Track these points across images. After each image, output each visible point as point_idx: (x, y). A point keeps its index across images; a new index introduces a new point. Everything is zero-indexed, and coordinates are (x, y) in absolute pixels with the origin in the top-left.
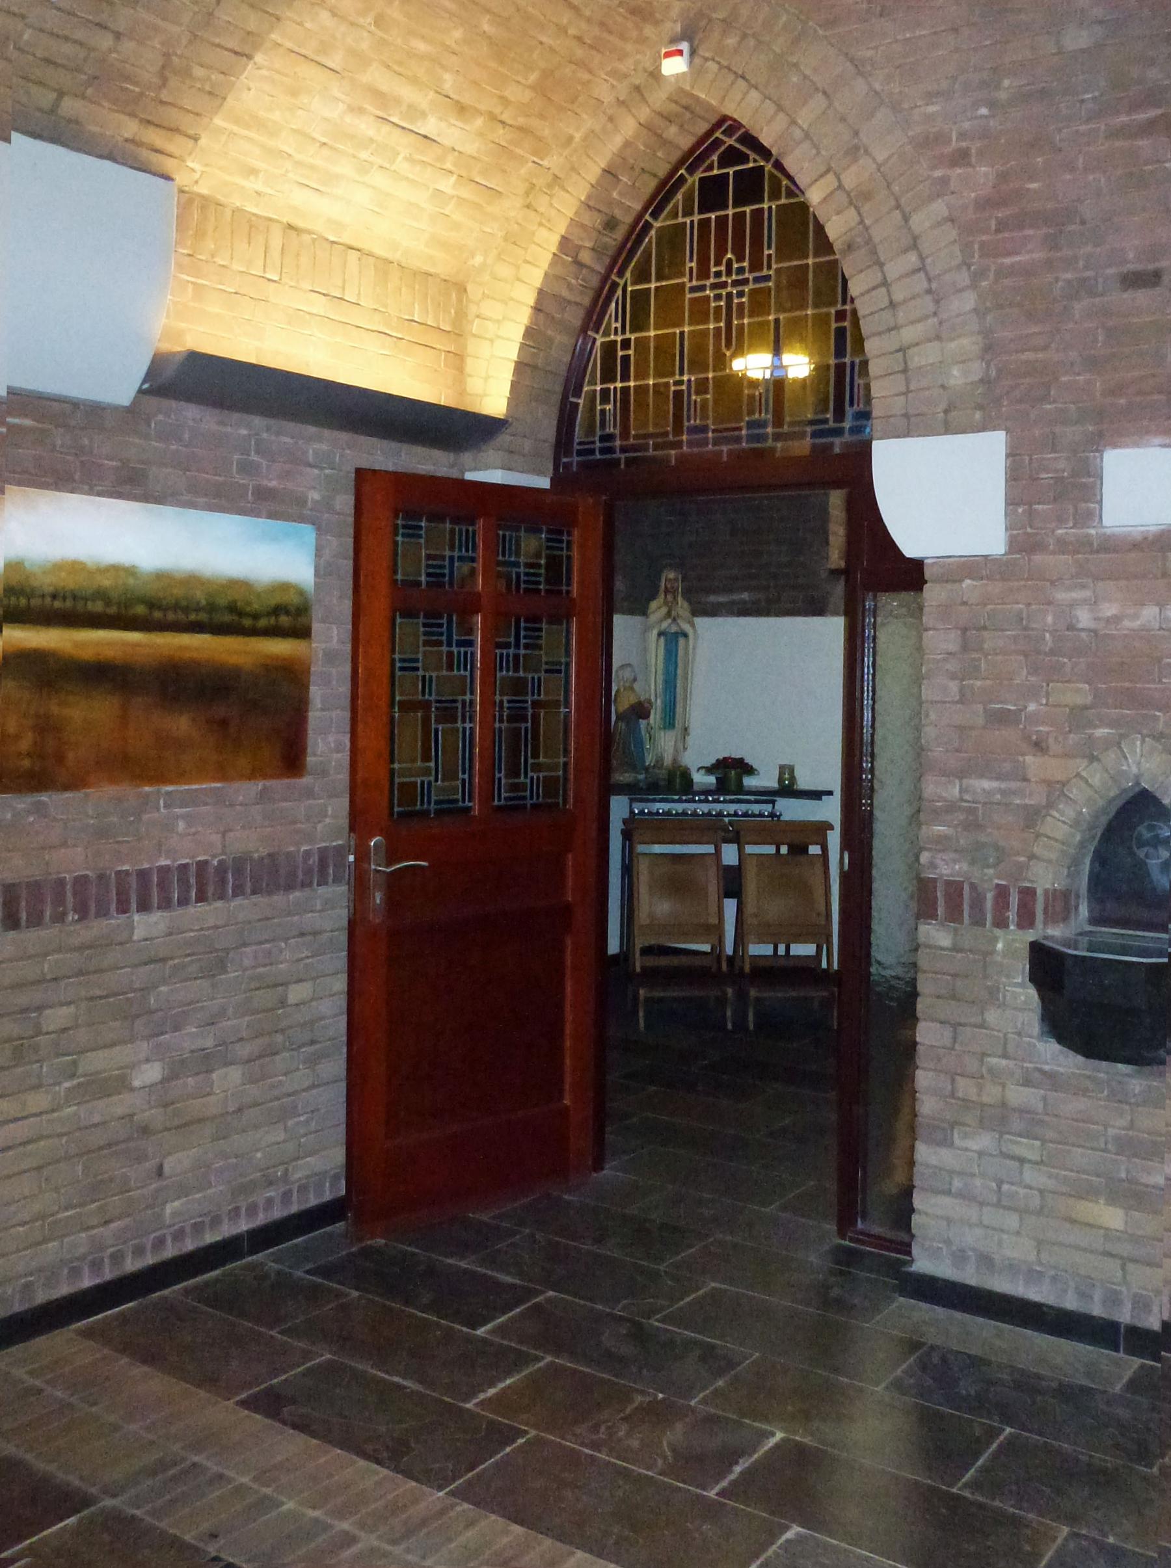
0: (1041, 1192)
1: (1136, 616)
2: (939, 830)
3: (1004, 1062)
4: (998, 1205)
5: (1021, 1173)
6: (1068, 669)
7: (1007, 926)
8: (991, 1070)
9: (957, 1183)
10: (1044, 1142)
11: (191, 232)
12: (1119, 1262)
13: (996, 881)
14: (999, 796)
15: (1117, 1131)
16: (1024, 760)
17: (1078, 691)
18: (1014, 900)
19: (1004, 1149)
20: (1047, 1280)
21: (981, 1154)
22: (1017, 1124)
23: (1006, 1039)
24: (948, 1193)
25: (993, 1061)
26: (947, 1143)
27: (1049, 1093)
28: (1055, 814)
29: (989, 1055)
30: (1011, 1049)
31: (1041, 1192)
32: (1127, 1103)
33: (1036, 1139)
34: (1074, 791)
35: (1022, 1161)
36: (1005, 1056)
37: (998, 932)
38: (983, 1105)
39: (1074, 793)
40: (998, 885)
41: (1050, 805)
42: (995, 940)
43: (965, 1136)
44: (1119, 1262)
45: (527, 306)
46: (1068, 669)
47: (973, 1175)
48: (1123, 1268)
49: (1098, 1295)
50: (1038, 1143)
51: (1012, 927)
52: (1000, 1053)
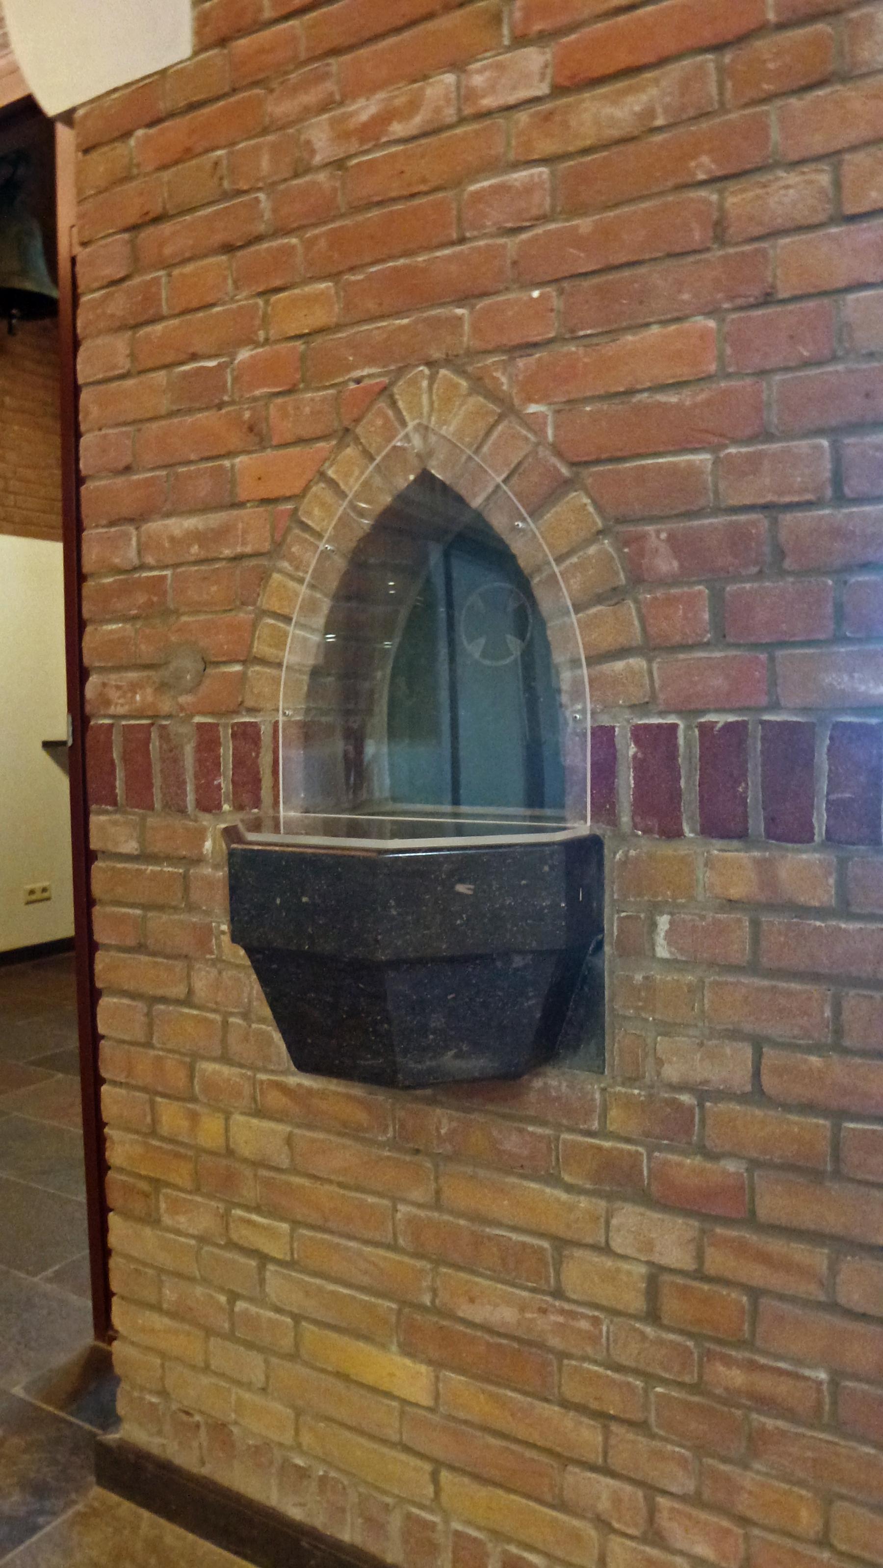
0: (297, 1318)
1: (413, 106)
2: (111, 632)
3: (226, 1071)
4: (231, 1336)
5: (262, 1281)
6: (299, 259)
7: (219, 807)
8: (209, 1086)
9: (170, 1295)
10: (295, 1223)
11: (28, 1438)
12: (428, 1467)
13: (198, 719)
14: (195, 549)
15: (414, 1210)
16: (233, 466)
17: (316, 298)
18: (227, 752)
19: (234, 1237)
20: (314, 1486)
21: (202, 1239)
22: (250, 1192)
23: (225, 1024)
24: (157, 1308)
25: (209, 1067)
26: (152, 1220)
27: (297, 1131)
28: (285, 565)
29: (204, 1058)
30: (235, 1046)
31: (297, 1318)
32: (428, 1154)
33: (283, 1219)
34: (316, 511)
35: (264, 1259)
36: (225, 1059)
37: (206, 819)
38: (201, 1150)
39: (314, 517)
40: (200, 726)
41: (278, 548)
42: (200, 835)
43: (175, 1207)
44: (428, 1467)
45: (108, 947)
46: (299, 259)
47: (191, 1279)
48: (435, 1478)
49: (395, 1523)
50: (285, 1227)
51: (226, 807)
52: (218, 1052)
